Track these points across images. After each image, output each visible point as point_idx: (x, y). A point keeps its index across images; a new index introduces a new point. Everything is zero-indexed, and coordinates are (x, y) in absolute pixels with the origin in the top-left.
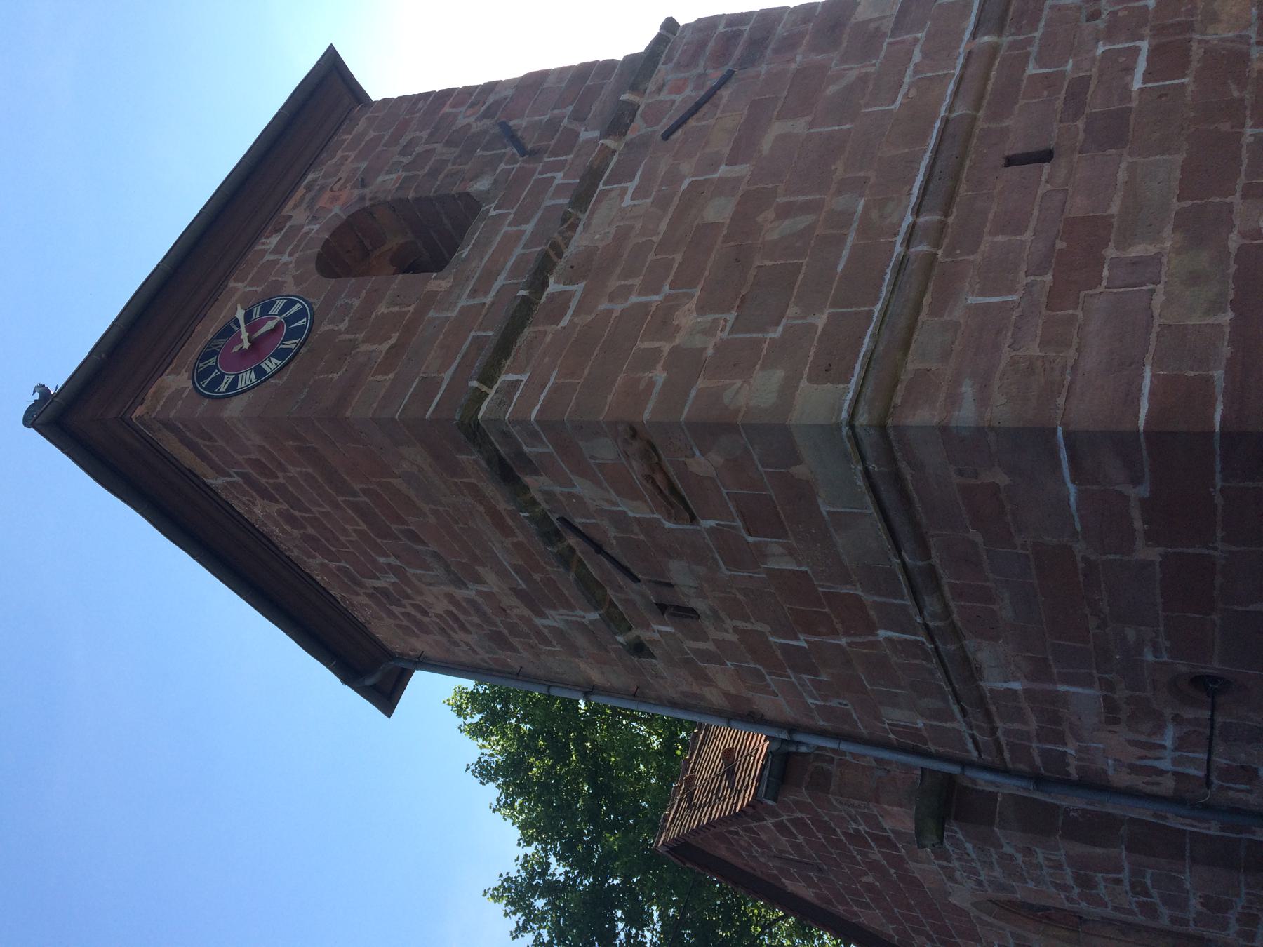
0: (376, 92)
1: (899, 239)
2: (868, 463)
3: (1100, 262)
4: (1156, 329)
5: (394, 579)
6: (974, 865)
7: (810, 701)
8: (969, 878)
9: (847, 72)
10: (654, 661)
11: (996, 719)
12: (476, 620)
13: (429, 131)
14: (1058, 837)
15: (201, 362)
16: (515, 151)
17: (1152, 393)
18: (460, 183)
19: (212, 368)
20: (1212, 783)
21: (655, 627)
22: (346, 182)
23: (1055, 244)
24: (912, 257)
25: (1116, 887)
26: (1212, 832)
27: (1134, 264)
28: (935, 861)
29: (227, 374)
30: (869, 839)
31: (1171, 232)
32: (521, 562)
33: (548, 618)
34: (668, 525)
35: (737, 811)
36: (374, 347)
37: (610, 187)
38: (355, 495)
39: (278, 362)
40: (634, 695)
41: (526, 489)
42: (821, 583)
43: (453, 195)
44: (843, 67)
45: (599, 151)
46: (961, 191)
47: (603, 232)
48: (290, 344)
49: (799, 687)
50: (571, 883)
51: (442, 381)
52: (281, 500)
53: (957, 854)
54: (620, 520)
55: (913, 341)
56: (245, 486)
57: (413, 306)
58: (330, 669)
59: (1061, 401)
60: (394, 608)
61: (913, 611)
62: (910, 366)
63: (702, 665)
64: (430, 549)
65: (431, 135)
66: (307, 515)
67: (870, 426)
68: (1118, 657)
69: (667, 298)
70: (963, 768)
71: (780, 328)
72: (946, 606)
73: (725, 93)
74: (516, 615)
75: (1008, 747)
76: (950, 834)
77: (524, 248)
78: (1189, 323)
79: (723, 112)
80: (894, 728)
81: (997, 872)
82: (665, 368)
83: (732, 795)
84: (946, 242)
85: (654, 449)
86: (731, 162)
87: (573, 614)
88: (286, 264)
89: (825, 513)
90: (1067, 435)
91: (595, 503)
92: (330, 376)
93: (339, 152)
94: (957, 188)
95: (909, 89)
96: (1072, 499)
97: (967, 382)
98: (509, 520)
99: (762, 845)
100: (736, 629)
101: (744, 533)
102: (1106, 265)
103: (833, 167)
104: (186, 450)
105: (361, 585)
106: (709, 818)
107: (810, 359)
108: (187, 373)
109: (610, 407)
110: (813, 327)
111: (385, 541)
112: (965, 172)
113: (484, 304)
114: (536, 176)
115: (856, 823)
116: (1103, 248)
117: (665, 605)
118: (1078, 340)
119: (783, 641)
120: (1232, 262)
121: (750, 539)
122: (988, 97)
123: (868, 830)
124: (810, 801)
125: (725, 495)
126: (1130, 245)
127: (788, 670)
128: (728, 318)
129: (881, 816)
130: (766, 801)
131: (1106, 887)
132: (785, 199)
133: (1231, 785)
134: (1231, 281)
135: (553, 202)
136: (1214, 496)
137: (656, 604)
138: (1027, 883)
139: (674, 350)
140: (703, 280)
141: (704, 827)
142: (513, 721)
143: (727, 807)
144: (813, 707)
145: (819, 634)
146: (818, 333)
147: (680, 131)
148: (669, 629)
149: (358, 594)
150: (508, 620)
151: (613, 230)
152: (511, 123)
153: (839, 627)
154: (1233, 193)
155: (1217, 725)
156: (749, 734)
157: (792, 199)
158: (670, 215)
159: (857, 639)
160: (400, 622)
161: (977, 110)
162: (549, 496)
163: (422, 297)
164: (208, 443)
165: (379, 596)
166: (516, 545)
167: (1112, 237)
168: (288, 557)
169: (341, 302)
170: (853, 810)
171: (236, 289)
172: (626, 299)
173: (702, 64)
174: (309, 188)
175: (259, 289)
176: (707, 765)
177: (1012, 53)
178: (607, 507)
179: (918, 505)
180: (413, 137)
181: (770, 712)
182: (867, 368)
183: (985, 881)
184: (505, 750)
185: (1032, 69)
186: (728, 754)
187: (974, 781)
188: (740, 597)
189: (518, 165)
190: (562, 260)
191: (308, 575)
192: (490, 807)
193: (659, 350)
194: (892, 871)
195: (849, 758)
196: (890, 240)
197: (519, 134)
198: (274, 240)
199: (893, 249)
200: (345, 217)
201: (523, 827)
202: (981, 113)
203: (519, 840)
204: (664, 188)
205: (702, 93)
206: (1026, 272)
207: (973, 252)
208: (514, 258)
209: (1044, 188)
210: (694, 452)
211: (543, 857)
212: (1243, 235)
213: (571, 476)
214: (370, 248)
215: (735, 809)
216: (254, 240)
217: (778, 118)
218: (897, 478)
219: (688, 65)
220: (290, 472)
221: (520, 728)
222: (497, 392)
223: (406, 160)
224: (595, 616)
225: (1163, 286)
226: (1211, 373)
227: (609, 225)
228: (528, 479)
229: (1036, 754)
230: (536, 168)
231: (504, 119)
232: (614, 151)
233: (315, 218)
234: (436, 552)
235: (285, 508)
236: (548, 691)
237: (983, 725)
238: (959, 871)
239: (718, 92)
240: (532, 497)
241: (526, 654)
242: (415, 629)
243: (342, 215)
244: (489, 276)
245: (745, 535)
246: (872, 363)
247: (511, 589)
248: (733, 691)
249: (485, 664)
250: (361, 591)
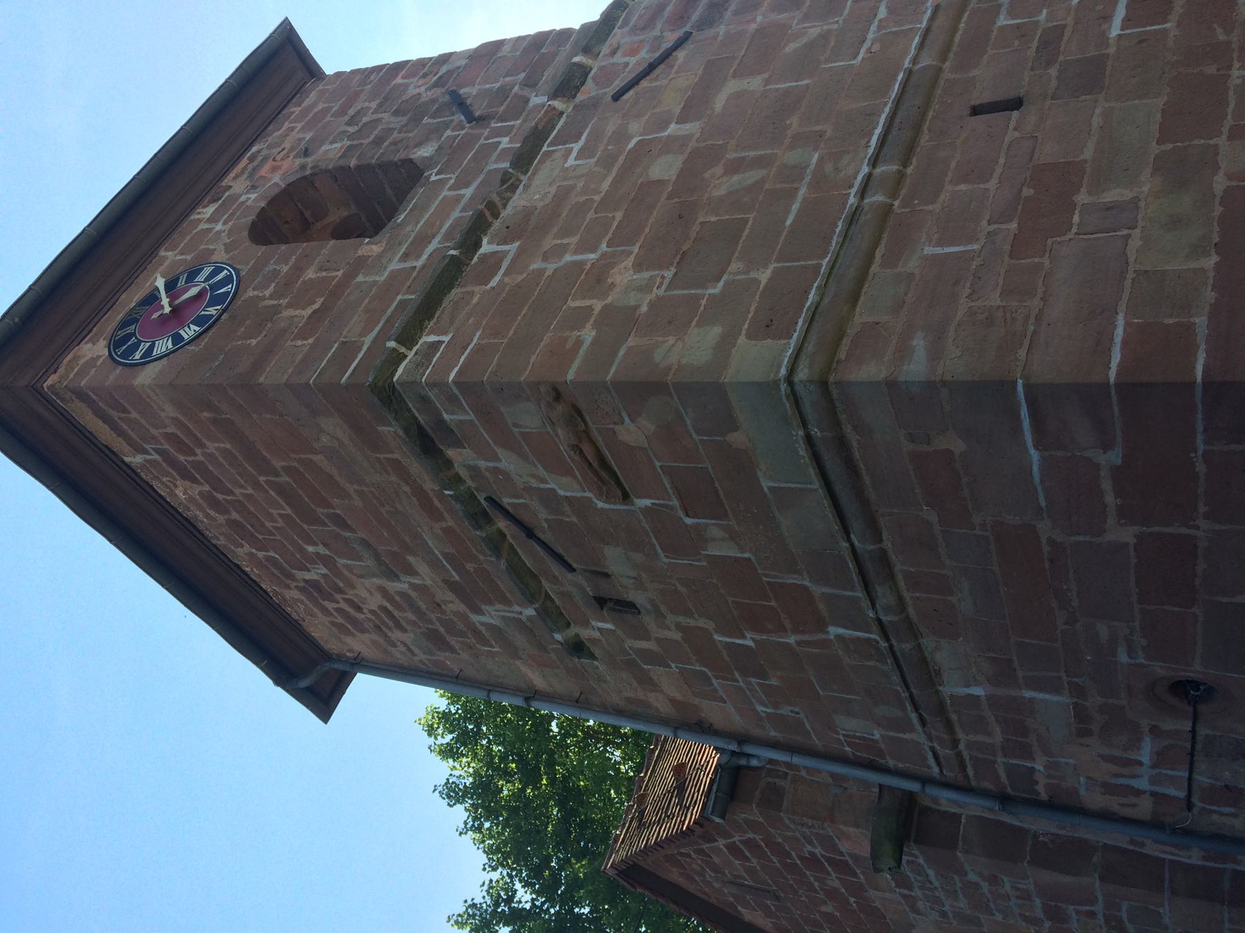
1: (853, 191)
2: (810, 427)
4: (1131, 275)
5: (324, 571)
6: (937, 894)
7: (760, 708)
8: (932, 909)
9: (808, 30)
10: (596, 663)
11: (958, 729)
12: (410, 616)
14: (1026, 864)
15: (120, 329)
16: (463, 118)
17: (1125, 342)
18: (404, 150)
20: (1194, 806)
21: (594, 623)
22: (290, 151)
23: (1021, 191)
24: (866, 208)
27: (1108, 209)
29: (144, 342)
30: (826, 864)
32: (452, 550)
34: (600, 505)
36: (297, 312)
38: (277, 475)
39: (197, 329)
40: (577, 701)
41: (449, 463)
42: (767, 572)
43: (395, 162)
45: (546, 112)
46: (922, 141)
47: (542, 192)
48: (212, 311)
50: (537, 911)
51: (362, 345)
53: (920, 882)
54: (549, 499)
55: (863, 293)
56: (164, 464)
57: (342, 271)
59: (1022, 353)
60: (326, 604)
61: (865, 603)
63: (645, 667)
64: (359, 535)
65: (380, 105)
66: (229, 498)
67: (810, 381)
69: (604, 255)
71: (721, 284)
72: (901, 599)
73: (681, 55)
76: (910, 858)
77: (461, 211)
78: (1168, 268)
80: (849, 739)
81: (962, 903)
83: (681, 813)
84: (903, 192)
85: (580, 413)
86: (682, 120)
87: (511, 609)
88: (219, 233)
89: (766, 489)
90: (1028, 388)
91: (522, 480)
92: (248, 342)
93: (287, 123)
94: (918, 139)
95: (872, 44)
96: (1035, 468)
97: (920, 334)
98: (436, 502)
99: (716, 870)
101: (681, 513)
102: (1077, 212)
103: (788, 122)
104: (101, 423)
105: (291, 577)
107: (750, 316)
108: (105, 342)
109: (532, 367)
110: (756, 281)
113: (415, 267)
114: (482, 141)
115: (811, 845)
116: (1074, 195)
118: (1044, 289)
119: (728, 640)
121: (688, 521)
122: (955, 48)
123: (824, 853)
124: (761, 820)
126: (1103, 191)
127: (736, 673)
129: (838, 838)
132: (735, 155)
134: (1215, 224)
135: (496, 166)
136: (1196, 462)
139: (605, 308)
141: (651, 847)
142: (484, 742)
143: (674, 825)
144: (764, 715)
147: (631, 92)
148: (609, 626)
151: (553, 190)
152: (462, 91)
153: (787, 623)
154: (1219, 134)
155: (1199, 738)
156: (699, 744)
157: (743, 154)
158: (613, 174)
159: (806, 637)
162: (475, 471)
163: (351, 262)
165: (311, 590)
166: (445, 530)
168: (215, 546)
169: (271, 267)
170: (807, 830)
171: (166, 258)
173: (659, 26)
174: (251, 159)
175: (189, 257)
176: (660, 782)
177: (981, 6)
179: (867, 479)
180: (362, 108)
182: (811, 321)
183: (949, 913)
184: (476, 774)
185: (1003, 20)
186: (679, 769)
187: (935, 800)
188: (683, 590)
189: (463, 132)
192: (457, 830)
194: (852, 900)
195: (803, 773)
196: (844, 192)
197: (469, 102)
198: (210, 210)
200: (283, 186)
201: (489, 851)
202: (947, 64)
204: (609, 148)
205: (657, 55)
206: (989, 221)
207: (933, 202)
208: (450, 222)
209: (1011, 135)
210: (622, 418)
211: (508, 883)
212: (1230, 177)
214: (310, 220)
216: (192, 208)
217: (734, 77)
218: (842, 445)
219: (644, 29)
221: (492, 750)
222: (416, 354)
223: (351, 129)
224: (530, 612)
225: (1140, 231)
226: (1192, 320)
227: (550, 185)
228: (451, 453)
232: (561, 113)
233: (254, 187)
234: (364, 540)
235: (207, 489)
236: (488, 696)
237: (944, 736)
238: (922, 900)
239: (674, 54)
240: (456, 473)
241: (465, 656)
243: (281, 183)
244: (423, 239)
246: (817, 316)
247: (445, 581)
248: (678, 696)
249: (424, 667)
250: (293, 584)
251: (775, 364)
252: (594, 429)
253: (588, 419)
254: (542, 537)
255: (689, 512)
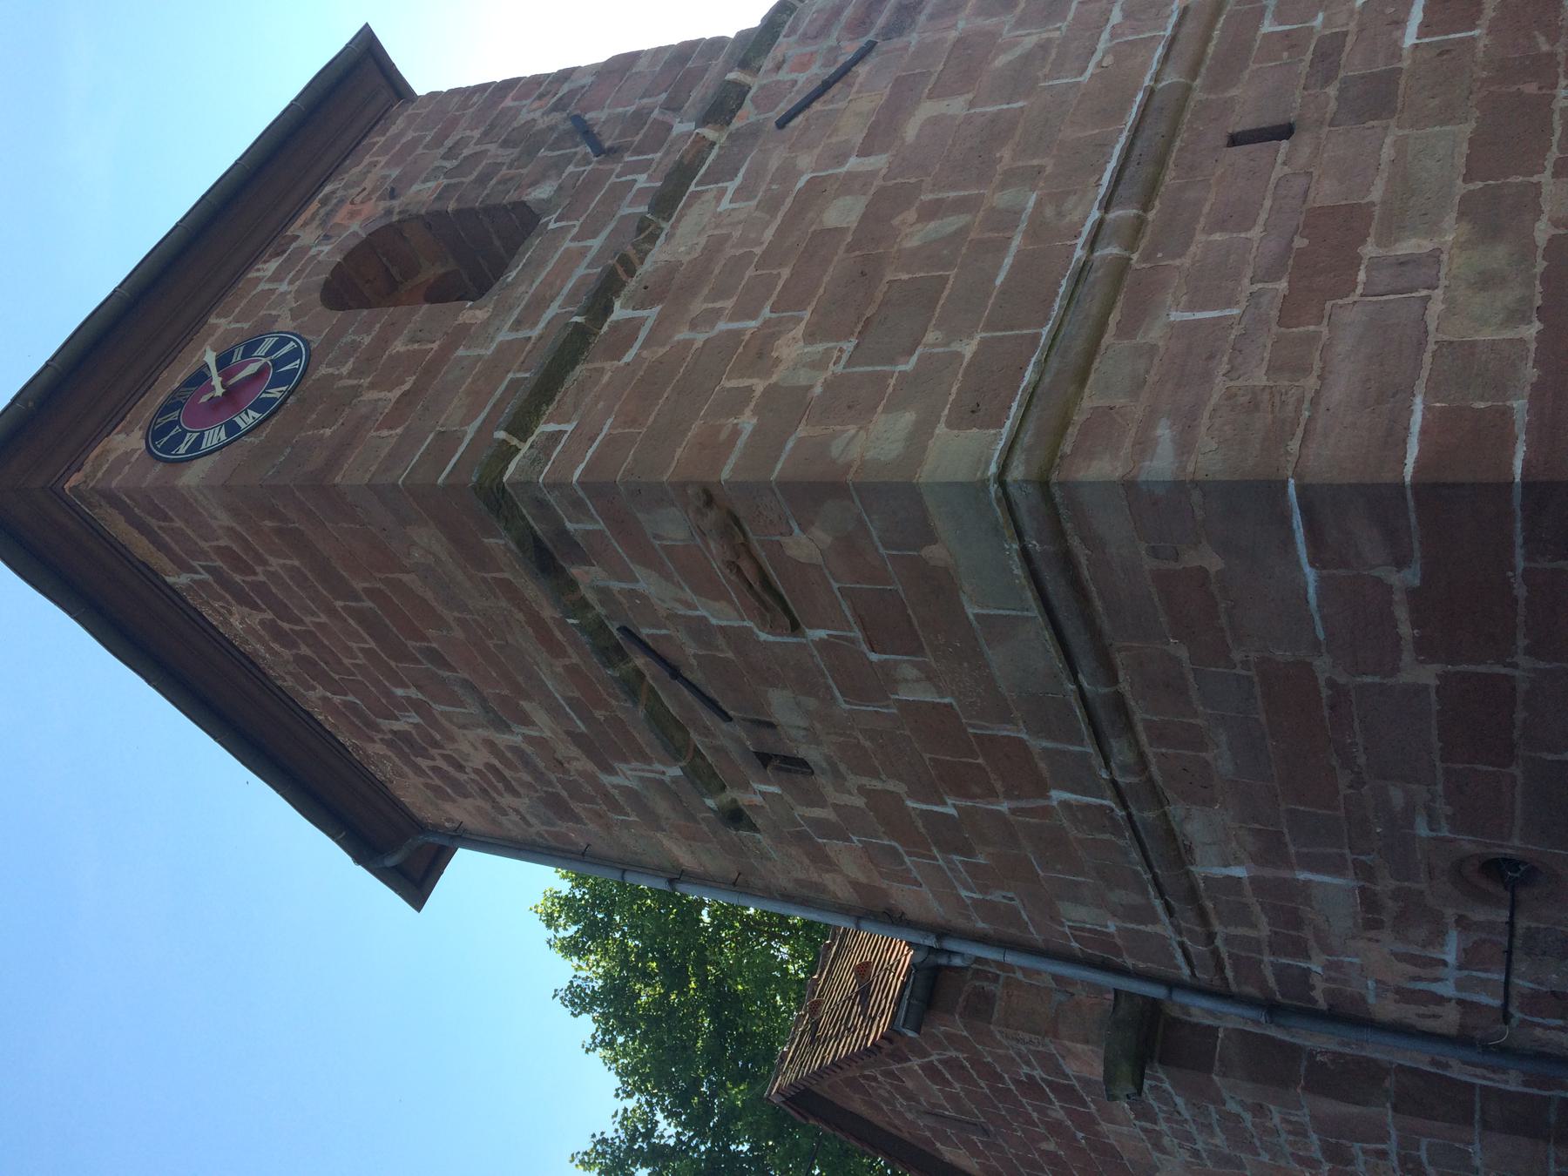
0: (421, 87)
1: (1081, 241)
3: (1355, 262)
4: (1431, 347)
5: (417, 720)
7: (964, 893)
8: (1181, 1147)
10: (758, 835)
12: (527, 778)
13: (482, 129)
14: (1299, 1091)
15: (159, 417)
17: (1424, 431)
19: (172, 424)
20: (1512, 1016)
21: (755, 786)
25: (1380, 1162)
26: (1512, 1087)
28: (1137, 1122)
31: (1454, 222)
32: (577, 694)
33: (617, 774)
34: (763, 636)
35: (869, 1045)
36: (382, 395)
37: (703, 188)
38: (357, 598)
39: (257, 415)
40: (734, 884)
41: (572, 584)
44: (1018, 33)
45: (694, 141)
46: (1167, 178)
48: (275, 393)
49: (949, 874)
51: (464, 436)
52: (264, 607)
54: (700, 630)
55: (1093, 370)
57: (438, 343)
58: (338, 842)
59: (1294, 446)
60: (419, 760)
61: (1097, 761)
62: (1086, 404)
63: (820, 840)
65: (485, 134)
66: (297, 628)
67: (1026, 481)
68: (1379, 830)
69: (766, 323)
70: (1170, 991)
72: (1141, 755)
73: (862, 70)
74: (577, 770)
75: (1231, 961)
76: (1154, 1083)
79: (858, 92)
80: (1077, 933)
81: (1219, 1140)
82: (754, 413)
84: (1144, 243)
86: (864, 152)
88: (283, 294)
89: (971, 617)
90: (1302, 490)
91: (666, 606)
93: (368, 156)
95: (1104, 56)
96: (1311, 591)
99: (910, 1097)
100: (862, 790)
101: (864, 647)
102: (1362, 267)
103: (998, 155)
104: (136, 534)
105: (378, 730)
106: (835, 1056)
110: (959, 356)
111: (400, 665)
112: (1174, 155)
113: (530, 338)
114: (613, 179)
117: (767, 754)
119: (925, 807)
120: (1539, 259)
121: (874, 657)
124: (965, 1033)
125: (836, 591)
128: (845, 348)
129: (1063, 1057)
130: (905, 1030)
131: (1366, 1163)
132: (931, 197)
133: (1537, 1020)
134: (1537, 282)
137: (755, 753)
138: (1259, 1155)
139: (770, 391)
140: (816, 300)
142: (617, 935)
143: (856, 1041)
144: (969, 902)
145: (973, 797)
146: (965, 364)
147: (801, 117)
149: (373, 741)
150: (566, 777)
151: (703, 240)
152: (587, 117)
153: (999, 786)
157: (940, 195)
159: (1023, 804)
160: (429, 781)
161: (1194, 79)
162: (605, 594)
164: (163, 524)
167: (1372, 231)
168: (279, 688)
169: (348, 338)
170: (1023, 1048)
171: (216, 327)
172: (713, 327)
173: (835, 34)
174: (324, 202)
175: (246, 326)
178: (682, 611)
179: (1098, 604)
181: (912, 909)
184: (607, 975)
185: (1268, 27)
186: (863, 970)
187: (1185, 1008)
190: (635, 278)
191: (308, 713)
193: (750, 389)
194: (1080, 1135)
195: (1019, 975)
197: (596, 130)
198: (273, 265)
199: (1073, 255)
200: (364, 236)
202: (1198, 82)
203: (617, 1090)
204: (774, 187)
205: (833, 70)
209: (1279, 171)
212: (1556, 223)
213: (631, 566)
214: (398, 278)
215: (866, 1043)
218: (1067, 561)
219: (816, 37)
220: (271, 565)
221: (627, 945)
222: (531, 447)
223: (449, 165)
224: (675, 771)
226: (1508, 403)
227: (699, 234)
228: (575, 571)
229: (1268, 973)
230: (613, 170)
231: (578, 112)
232: (713, 144)
233: (327, 237)
239: (854, 69)
242: (449, 790)
243: (360, 233)
244: (539, 304)
245: (866, 651)
246: (1035, 400)
247: (568, 733)
248: (863, 879)
250: (378, 737)
251: (983, 459)
252: (755, 542)
253: (747, 528)
254: (690, 677)
255: (875, 646)
